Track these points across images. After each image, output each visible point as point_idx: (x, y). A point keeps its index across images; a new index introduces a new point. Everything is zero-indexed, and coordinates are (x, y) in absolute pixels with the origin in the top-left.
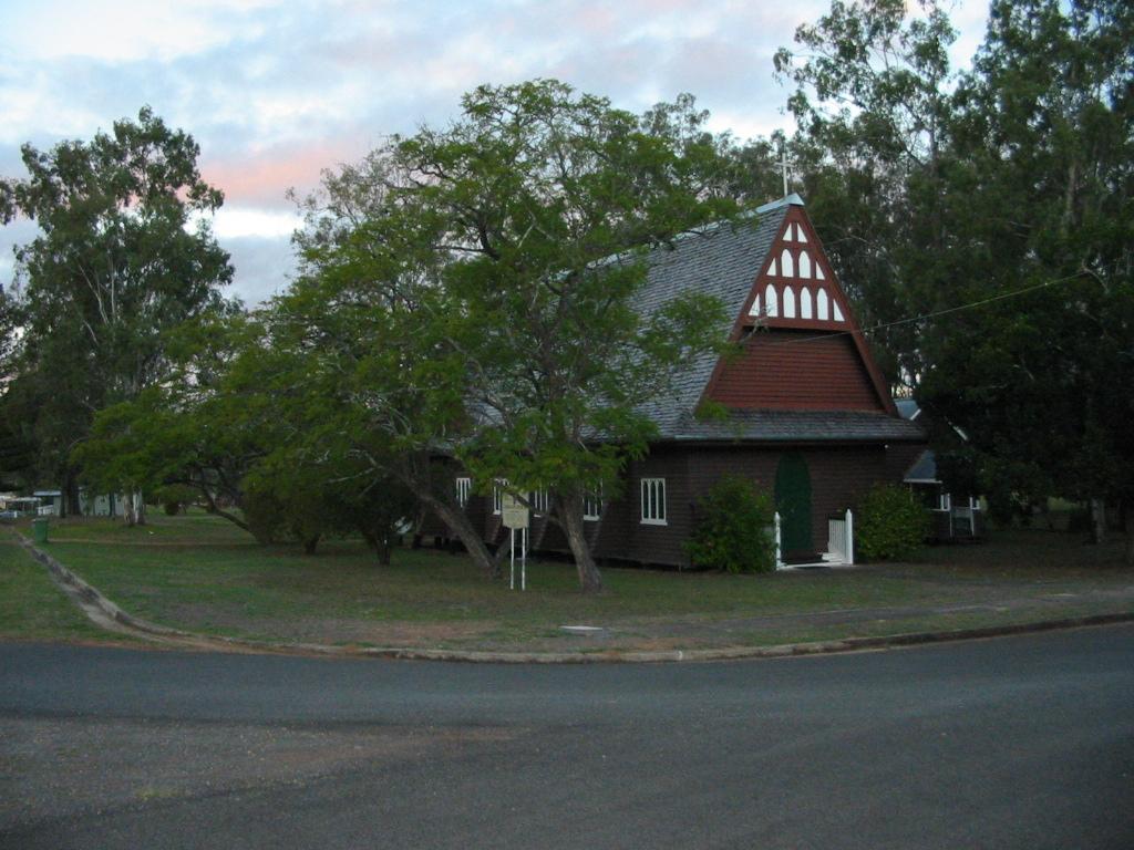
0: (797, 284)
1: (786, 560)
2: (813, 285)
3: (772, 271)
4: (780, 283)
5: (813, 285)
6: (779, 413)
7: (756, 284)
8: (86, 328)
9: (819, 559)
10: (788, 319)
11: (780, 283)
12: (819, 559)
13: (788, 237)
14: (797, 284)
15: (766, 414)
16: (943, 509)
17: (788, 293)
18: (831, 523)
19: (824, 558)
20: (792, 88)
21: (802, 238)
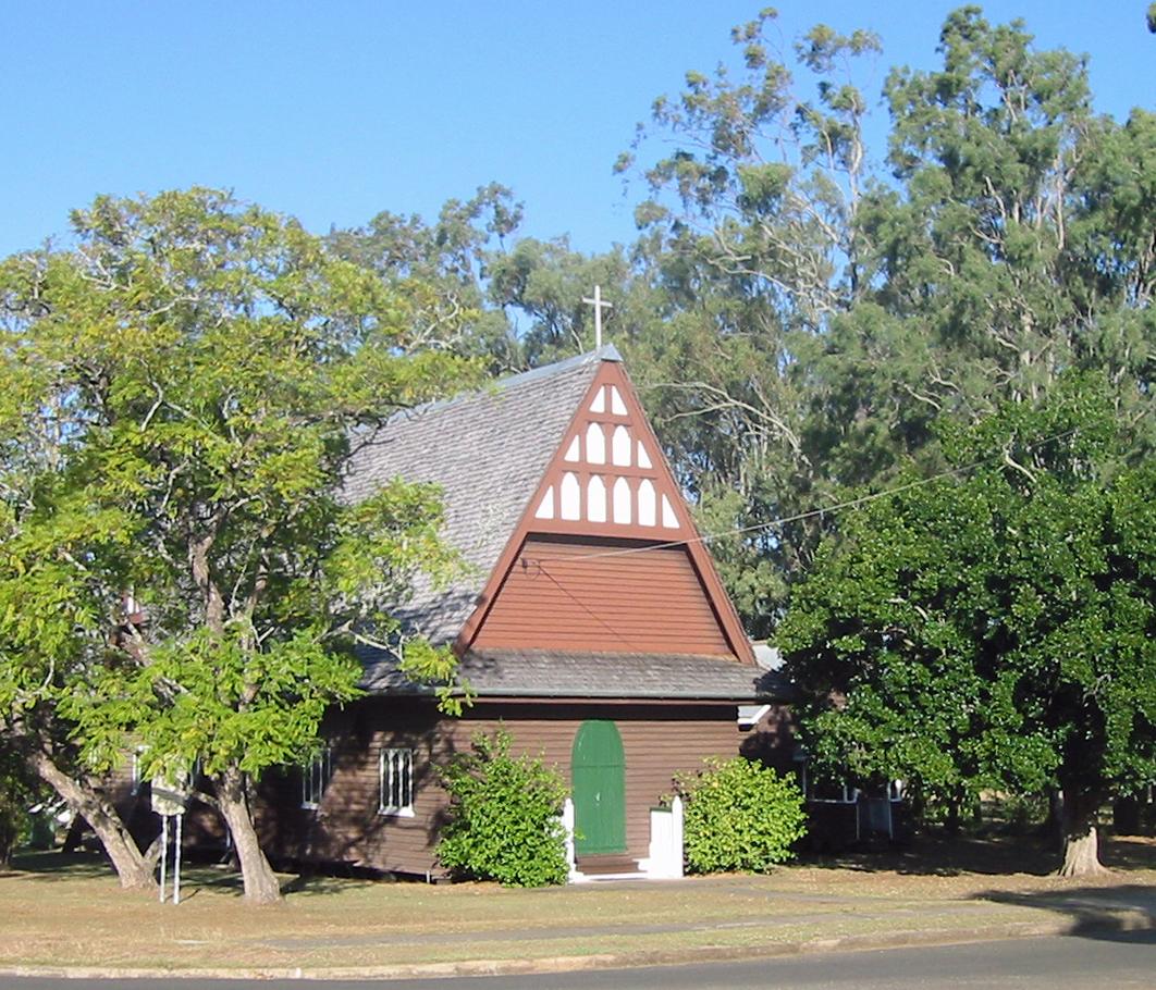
0: (609, 473)
1: (582, 866)
2: (634, 475)
3: (572, 455)
4: (584, 471)
5: (634, 475)
6: (578, 658)
7: (547, 473)
8: (151, 401)
9: (633, 867)
10: (567, 521)
11: (584, 471)
12: (633, 867)
13: (598, 406)
14: (609, 473)
15: (557, 658)
16: (846, 801)
17: (621, 486)
18: (1154, 883)
19: (640, 867)
20: (641, 192)
21: (619, 408)
